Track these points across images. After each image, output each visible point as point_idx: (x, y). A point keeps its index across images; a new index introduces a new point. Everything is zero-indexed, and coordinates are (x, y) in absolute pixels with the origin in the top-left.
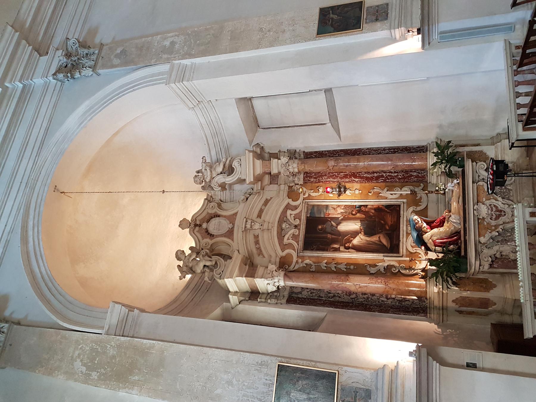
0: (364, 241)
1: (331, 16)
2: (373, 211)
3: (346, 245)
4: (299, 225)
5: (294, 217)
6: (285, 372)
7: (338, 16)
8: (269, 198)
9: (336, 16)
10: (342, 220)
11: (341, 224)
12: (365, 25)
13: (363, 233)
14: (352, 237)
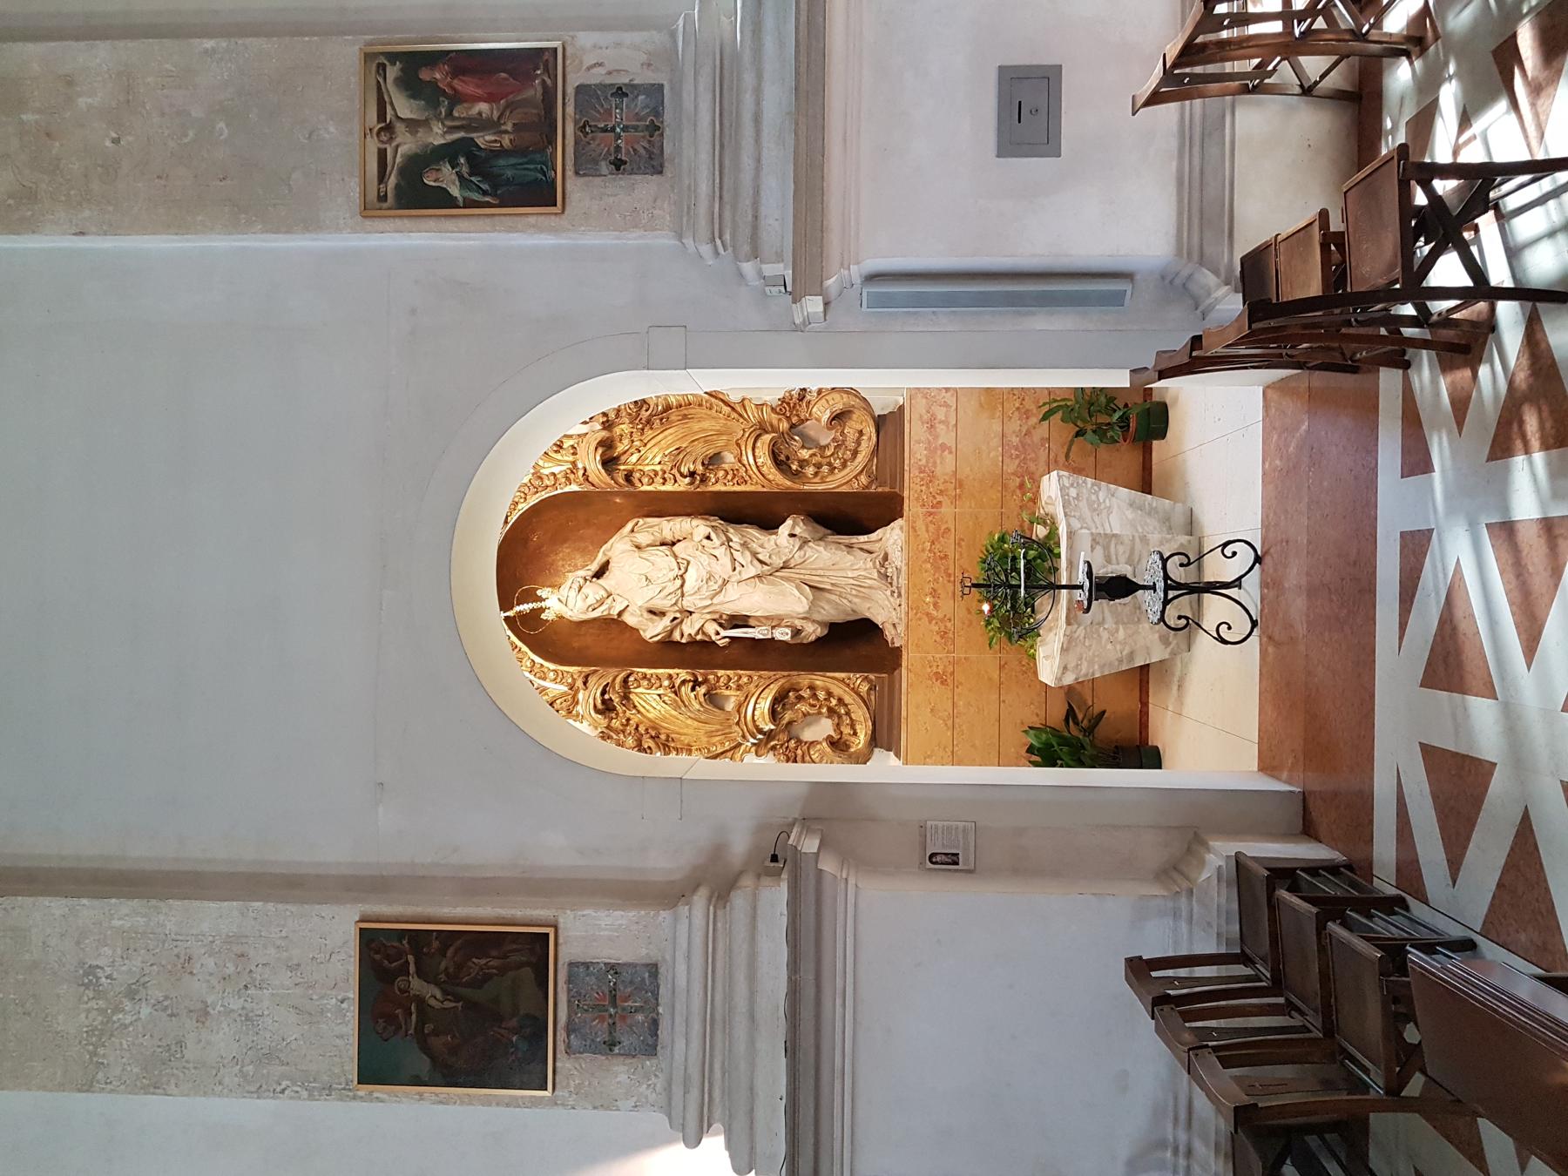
1: (417, 985)
6: (100, 978)
7: (445, 992)
9: (439, 994)
12: (565, 1064)
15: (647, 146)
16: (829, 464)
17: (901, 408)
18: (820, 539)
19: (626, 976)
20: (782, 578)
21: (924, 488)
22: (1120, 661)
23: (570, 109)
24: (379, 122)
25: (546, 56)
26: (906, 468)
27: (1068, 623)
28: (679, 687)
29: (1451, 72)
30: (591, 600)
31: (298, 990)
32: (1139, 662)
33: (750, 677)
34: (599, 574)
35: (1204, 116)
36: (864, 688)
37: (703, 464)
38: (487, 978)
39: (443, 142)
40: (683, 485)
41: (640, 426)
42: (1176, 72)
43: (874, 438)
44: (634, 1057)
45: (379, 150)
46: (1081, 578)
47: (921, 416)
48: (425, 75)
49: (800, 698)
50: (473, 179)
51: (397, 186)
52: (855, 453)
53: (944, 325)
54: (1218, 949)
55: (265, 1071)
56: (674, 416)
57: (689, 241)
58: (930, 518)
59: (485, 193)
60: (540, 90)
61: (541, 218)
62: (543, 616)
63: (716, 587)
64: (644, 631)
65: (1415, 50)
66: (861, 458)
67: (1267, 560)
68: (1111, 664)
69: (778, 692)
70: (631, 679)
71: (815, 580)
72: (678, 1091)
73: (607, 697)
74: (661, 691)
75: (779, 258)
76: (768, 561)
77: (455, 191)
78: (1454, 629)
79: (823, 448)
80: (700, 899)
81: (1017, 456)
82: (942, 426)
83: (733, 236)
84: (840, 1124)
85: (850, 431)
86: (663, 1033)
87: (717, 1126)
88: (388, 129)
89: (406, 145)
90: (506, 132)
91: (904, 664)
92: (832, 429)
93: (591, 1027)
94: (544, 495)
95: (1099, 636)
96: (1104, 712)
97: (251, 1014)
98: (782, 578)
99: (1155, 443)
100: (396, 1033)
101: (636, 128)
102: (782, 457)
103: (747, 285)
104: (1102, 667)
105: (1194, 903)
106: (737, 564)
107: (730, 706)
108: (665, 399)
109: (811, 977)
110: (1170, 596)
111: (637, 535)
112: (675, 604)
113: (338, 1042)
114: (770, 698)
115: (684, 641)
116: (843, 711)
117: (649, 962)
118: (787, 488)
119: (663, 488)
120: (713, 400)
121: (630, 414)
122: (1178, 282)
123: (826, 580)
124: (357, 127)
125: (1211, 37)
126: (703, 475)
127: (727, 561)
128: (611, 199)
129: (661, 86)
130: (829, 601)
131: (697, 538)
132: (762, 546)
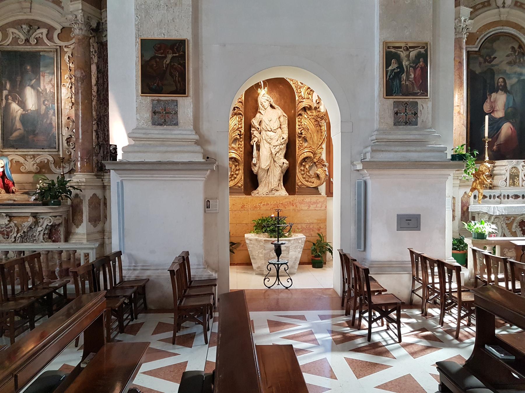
0: (15, 115)
1: (170, 56)
2: (48, 122)
3: (9, 97)
4: (31, 45)
5: (39, 37)
7: (168, 64)
8: (63, 5)
9: (168, 62)
10: (38, 91)
11: (32, 90)
13: (24, 112)
14: (18, 102)
15: (402, 121)
16: (304, 174)
17: (320, 194)
18: (282, 172)
19: (175, 116)
20: (271, 160)
21: (298, 201)
22: (252, 256)
23: (411, 100)
24: (409, 46)
25: (426, 93)
26: (303, 196)
27: (265, 240)
28: (239, 130)
29: (419, 321)
30: (264, 104)
31: (167, 22)
32: (252, 261)
33: (242, 151)
34: (272, 106)
35: (407, 267)
36: (239, 185)
37: (304, 137)
38: (172, 77)
39: (403, 65)
40: (298, 131)
41: (315, 118)
42: (419, 258)
43: (312, 187)
44: (152, 119)
45: (402, 47)
46: (280, 242)
47: (318, 200)
48: (421, 60)
49: (236, 166)
50: (393, 73)
51: (391, 52)
52: (307, 181)
53: (352, 202)
54: (192, 275)
55: (143, 11)
56: (318, 128)
57: (376, 133)
58: (289, 203)
59: (390, 76)
60: (417, 92)
61: (382, 92)
62: (259, 89)
63: (268, 141)
64: (254, 119)
65: (424, 314)
66: (306, 183)
67: (287, 290)
68: (252, 253)
69: (238, 159)
70: (241, 116)
71: (270, 170)
72: (143, 131)
73: (236, 108)
74: (237, 125)
75: (372, 157)
76: (276, 156)
77: (390, 68)
78: (284, 325)
79: (309, 172)
80: (197, 137)
81: (307, 227)
82: (315, 206)
83: (377, 145)
84: (139, 176)
85: (314, 180)
86: (159, 127)
87: (133, 142)
88: (407, 49)
89: (403, 54)
90: (406, 82)
91: (247, 196)
92: (314, 174)
93: (159, 107)
94: (295, 89)
95: (261, 249)
96: (234, 253)
97: (159, 7)
98: (271, 160)
99: (311, 265)
100: (156, 50)
101: (406, 118)
102: (306, 160)
103: (363, 149)
104: (251, 251)
105: (202, 269)
106: (275, 147)
107: (233, 145)
108: (323, 125)
109: (180, 168)
110: (275, 265)
111: (283, 117)
112: (263, 129)
113: (152, 33)
114: (236, 157)
115: (251, 131)
116: (232, 179)
117: (179, 122)
118: (297, 161)
119: (297, 125)
120: (323, 139)
121: (319, 115)
122: (363, 262)
123: (271, 173)
124: (408, 40)
125: (428, 265)
126: (301, 137)
127: (276, 144)
128: (387, 111)
129: (417, 125)
130: (264, 174)
131: (283, 135)
132: (280, 154)
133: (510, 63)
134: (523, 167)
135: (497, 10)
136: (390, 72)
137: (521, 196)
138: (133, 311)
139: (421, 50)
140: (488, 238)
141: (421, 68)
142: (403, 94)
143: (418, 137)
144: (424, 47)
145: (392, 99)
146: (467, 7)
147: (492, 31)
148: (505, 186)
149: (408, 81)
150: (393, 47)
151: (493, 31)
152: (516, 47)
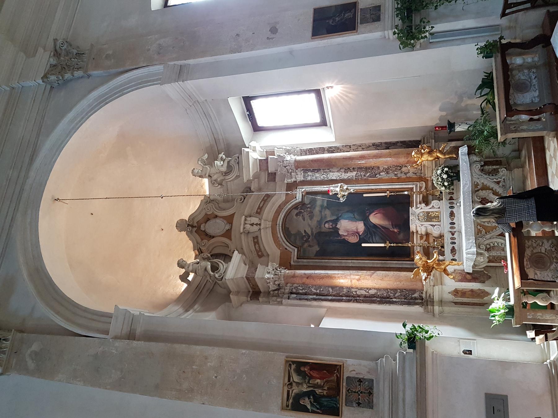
15: (368, 399)
39: (306, 390)
45: (288, 390)
48: (302, 369)
50: (314, 404)
51: (292, 403)
59: (318, 409)
77: (309, 407)
88: (291, 384)
89: (296, 390)
90: (325, 390)
101: (364, 393)
129: (373, 380)
133: (311, 218)
134: (418, 208)
135: (262, 231)
136: (314, 407)
137: (451, 209)
138: (557, 79)
139: (292, 369)
140: (512, 302)
141: (311, 370)
142: (338, 395)
143: (387, 384)
144: (289, 364)
145: (343, 408)
146: (256, 270)
147: (281, 236)
148: (439, 227)
149: (323, 387)
150: (287, 401)
151: (280, 234)
152: (296, 211)
